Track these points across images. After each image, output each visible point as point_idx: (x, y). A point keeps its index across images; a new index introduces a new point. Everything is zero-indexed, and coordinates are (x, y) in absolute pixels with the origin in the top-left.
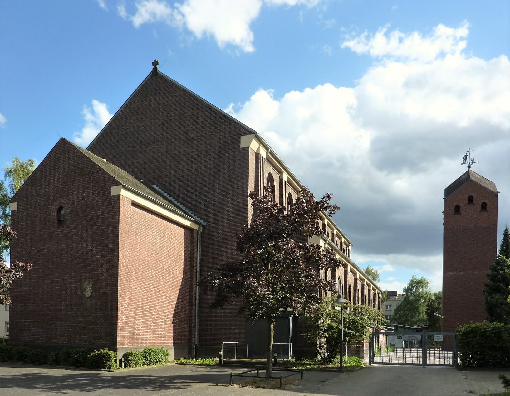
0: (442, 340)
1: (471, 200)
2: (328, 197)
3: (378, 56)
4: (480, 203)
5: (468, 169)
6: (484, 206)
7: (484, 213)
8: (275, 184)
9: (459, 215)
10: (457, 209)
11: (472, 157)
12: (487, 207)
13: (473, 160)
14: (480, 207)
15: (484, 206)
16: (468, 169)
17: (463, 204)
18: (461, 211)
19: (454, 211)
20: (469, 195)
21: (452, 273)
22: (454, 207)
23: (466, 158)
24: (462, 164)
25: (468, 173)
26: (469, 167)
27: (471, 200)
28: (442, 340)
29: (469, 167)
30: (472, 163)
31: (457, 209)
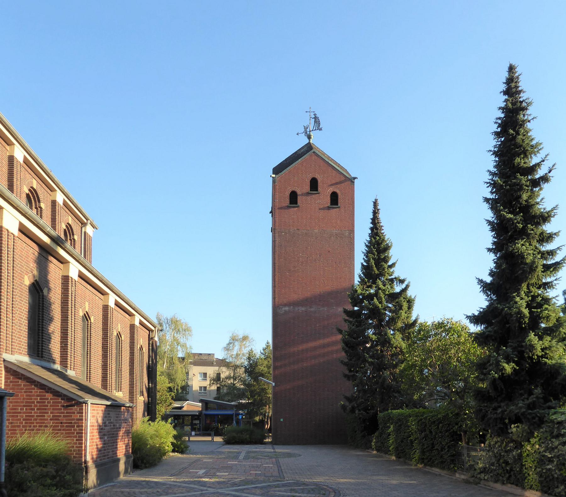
1: (314, 184)
6: (334, 199)
10: (294, 198)
15: (334, 199)
27: (314, 184)
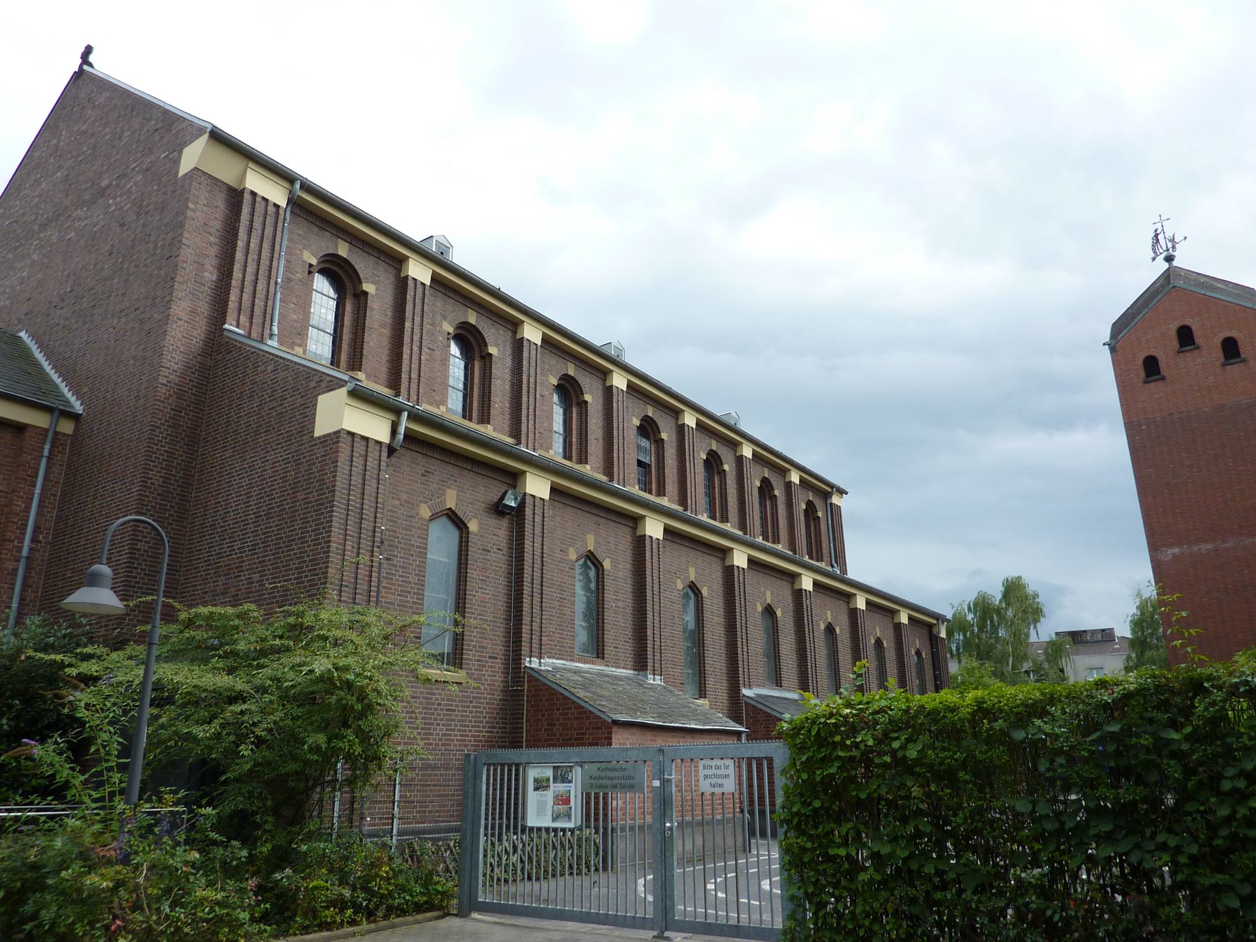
0: (532, 821)
1: (1186, 337)
2: (842, 492)
3: (983, 607)
4: (1217, 342)
5: (1166, 265)
7: (1235, 370)
8: (777, 492)
9: (1160, 383)
10: (1152, 367)
11: (1169, 234)
12: (1242, 350)
13: (1172, 240)
14: (1219, 354)
16: (1166, 265)
17: (1166, 351)
18: (1164, 370)
19: (1143, 374)
20: (1178, 324)
21: (1176, 550)
22: (1140, 361)
23: (1158, 241)
24: (1154, 259)
25: (1167, 276)
26: (1169, 259)
27: (1186, 337)
28: (532, 821)
29: (1169, 259)
30: (1174, 247)
31: (1152, 367)
